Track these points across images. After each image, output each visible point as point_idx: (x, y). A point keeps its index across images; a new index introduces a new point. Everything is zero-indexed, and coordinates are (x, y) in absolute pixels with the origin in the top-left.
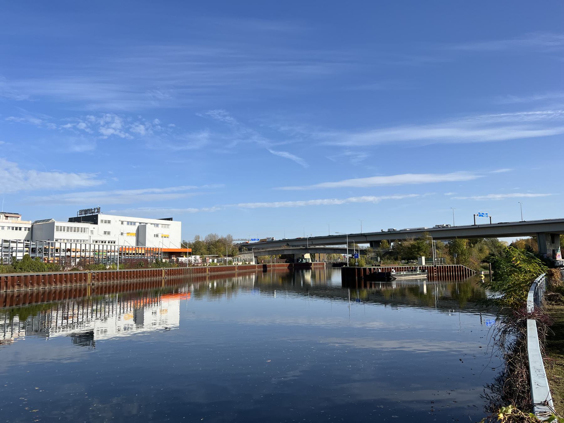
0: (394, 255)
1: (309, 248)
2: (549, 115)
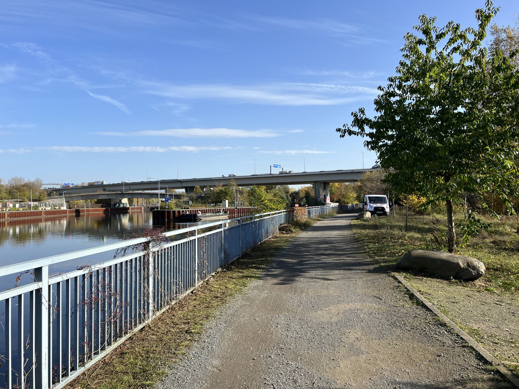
0: (205, 199)
1: (125, 192)
2: (332, 88)
